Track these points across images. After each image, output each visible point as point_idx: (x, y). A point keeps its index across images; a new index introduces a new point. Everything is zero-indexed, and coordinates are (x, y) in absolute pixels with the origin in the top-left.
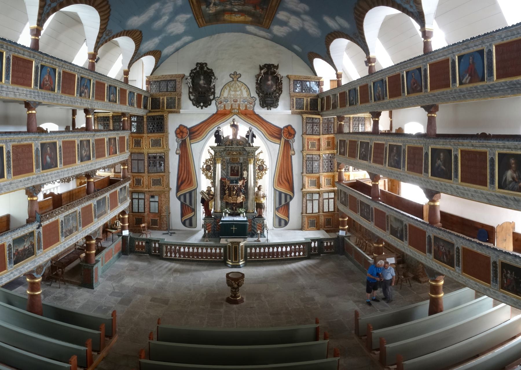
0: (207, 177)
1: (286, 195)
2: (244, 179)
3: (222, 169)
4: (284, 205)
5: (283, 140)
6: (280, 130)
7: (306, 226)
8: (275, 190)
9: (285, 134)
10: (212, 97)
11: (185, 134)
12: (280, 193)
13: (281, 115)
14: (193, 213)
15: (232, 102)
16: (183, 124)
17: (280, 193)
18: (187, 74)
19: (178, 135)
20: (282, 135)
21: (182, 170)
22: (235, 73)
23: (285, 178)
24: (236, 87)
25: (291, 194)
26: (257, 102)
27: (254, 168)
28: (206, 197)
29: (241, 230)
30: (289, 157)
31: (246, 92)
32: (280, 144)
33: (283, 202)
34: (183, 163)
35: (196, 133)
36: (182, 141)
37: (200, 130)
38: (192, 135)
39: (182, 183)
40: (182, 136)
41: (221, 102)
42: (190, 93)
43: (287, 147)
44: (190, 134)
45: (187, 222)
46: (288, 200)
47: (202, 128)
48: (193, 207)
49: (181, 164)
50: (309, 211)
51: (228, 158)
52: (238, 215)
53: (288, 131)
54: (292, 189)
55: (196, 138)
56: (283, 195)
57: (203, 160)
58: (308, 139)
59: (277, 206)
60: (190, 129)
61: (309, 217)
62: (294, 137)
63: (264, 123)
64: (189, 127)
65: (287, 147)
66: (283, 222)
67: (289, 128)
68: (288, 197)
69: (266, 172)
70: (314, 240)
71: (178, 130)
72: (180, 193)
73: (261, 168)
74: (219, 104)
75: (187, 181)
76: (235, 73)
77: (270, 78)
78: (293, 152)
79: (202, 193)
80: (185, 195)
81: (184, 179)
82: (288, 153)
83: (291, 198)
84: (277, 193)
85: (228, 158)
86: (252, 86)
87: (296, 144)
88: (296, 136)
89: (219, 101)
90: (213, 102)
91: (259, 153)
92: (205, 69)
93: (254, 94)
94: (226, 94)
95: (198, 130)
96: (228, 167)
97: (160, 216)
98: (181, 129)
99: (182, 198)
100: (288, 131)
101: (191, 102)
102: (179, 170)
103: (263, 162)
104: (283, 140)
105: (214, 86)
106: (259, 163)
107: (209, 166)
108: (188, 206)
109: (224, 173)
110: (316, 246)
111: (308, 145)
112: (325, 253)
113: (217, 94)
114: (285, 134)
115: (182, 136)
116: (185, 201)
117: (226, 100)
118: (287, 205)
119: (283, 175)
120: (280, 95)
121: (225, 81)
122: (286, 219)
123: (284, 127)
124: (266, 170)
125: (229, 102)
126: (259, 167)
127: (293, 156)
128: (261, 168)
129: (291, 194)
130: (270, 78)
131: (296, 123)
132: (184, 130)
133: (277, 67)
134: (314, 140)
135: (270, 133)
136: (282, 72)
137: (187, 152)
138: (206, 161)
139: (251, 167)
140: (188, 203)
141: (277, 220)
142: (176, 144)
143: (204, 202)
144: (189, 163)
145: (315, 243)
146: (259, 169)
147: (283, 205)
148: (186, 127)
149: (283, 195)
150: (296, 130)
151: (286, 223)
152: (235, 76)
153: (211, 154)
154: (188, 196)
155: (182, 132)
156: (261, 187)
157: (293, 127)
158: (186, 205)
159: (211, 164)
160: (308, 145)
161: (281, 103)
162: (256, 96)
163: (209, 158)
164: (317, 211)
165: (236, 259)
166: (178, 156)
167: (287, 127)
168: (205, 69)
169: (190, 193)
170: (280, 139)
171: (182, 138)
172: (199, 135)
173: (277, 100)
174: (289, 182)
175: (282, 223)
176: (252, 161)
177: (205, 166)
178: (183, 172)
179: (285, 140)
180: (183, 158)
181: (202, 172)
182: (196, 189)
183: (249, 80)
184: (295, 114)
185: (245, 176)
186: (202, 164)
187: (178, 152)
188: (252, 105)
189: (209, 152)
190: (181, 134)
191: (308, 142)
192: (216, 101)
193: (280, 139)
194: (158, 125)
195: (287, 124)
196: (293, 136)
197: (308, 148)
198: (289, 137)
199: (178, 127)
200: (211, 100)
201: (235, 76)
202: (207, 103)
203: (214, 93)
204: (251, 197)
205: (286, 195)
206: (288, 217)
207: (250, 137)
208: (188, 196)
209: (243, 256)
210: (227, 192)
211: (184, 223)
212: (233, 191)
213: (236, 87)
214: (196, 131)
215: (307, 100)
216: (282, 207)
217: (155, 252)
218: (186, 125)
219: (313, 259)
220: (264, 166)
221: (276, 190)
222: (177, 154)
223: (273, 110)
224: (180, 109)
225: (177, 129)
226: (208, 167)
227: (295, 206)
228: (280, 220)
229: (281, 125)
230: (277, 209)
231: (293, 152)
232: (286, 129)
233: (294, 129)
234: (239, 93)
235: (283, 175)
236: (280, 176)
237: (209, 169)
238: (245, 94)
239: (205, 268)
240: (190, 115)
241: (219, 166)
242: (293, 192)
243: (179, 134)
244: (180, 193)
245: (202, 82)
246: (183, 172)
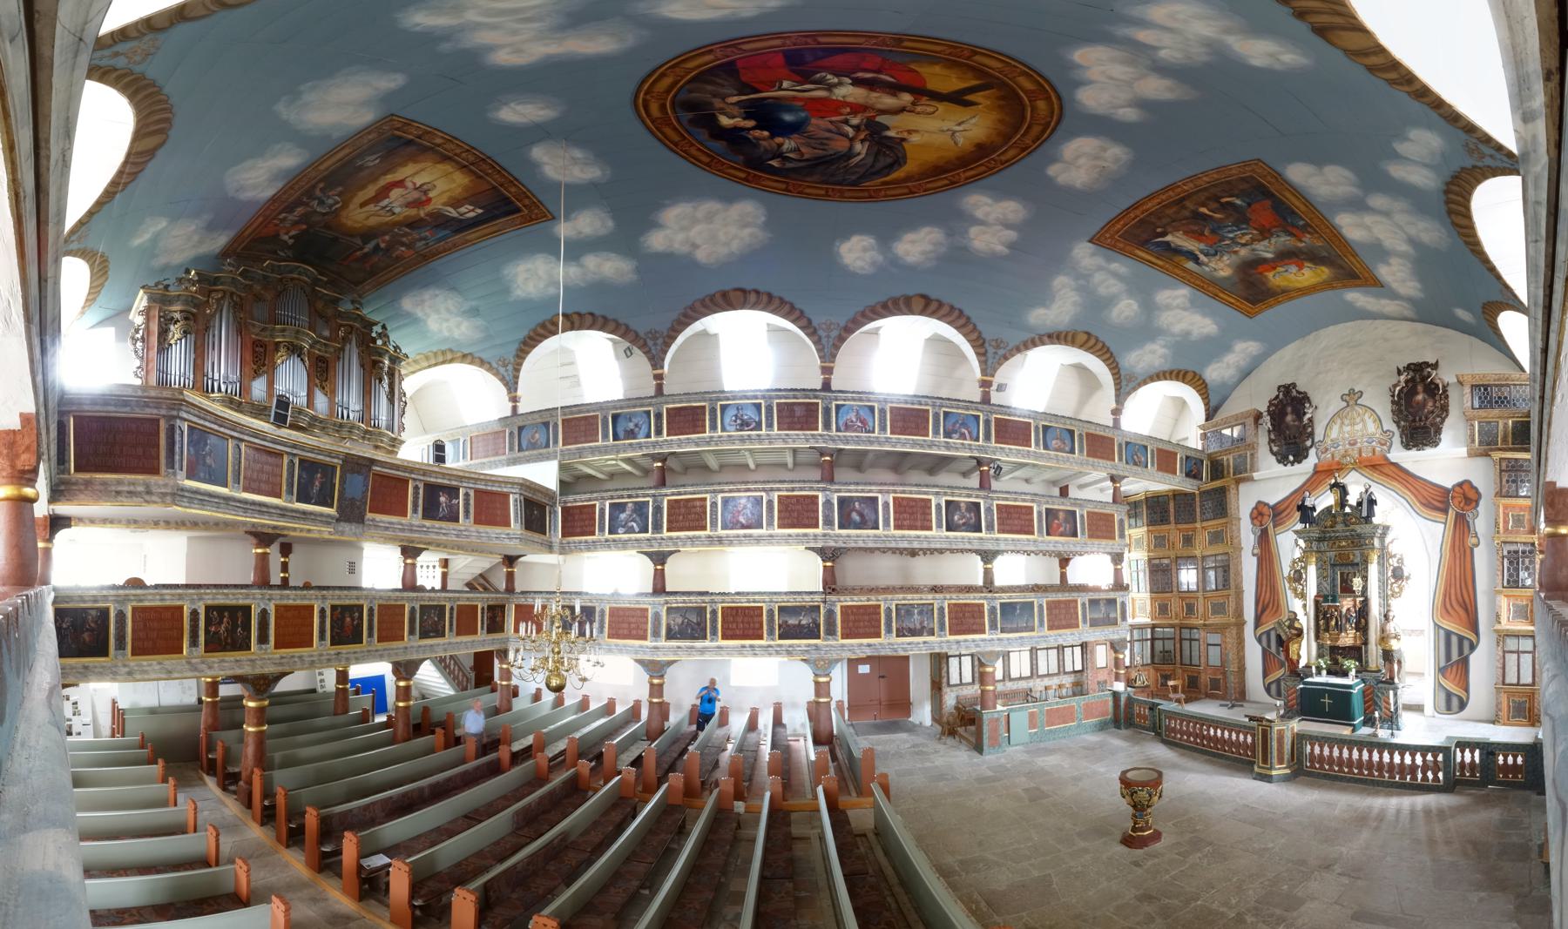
1: (1461, 639)
3: (1321, 577)
5: (1451, 514)
6: (1446, 491)
7: (1504, 714)
8: (1437, 627)
10: (1309, 443)
12: (1448, 634)
13: (1447, 459)
17: (1448, 634)
18: (1263, 408)
20: (1452, 504)
22: (1352, 392)
23: (1458, 599)
24: (1354, 420)
25: (1472, 637)
26: (1397, 439)
27: (1382, 572)
29: (1335, 706)
31: (1373, 424)
33: (1455, 656)
39: (1263, 611)
42: (1271, 441)
43: (1462, 526)
44: (1275, 516)
45: (1274, 687)
46: (1466, 651)
50: (1511, 678)
51: (1332, 554)
52: (1345, 674)
54: (1474, 627)
56: (1454, 640)
58: (1506, 507)
59: (1443, 664)
60: (1274, 508)
61: (1510, 694)
63: (1411, 480)
64: (1272, 502)
65: (1462, 526)
66: (1455, 702)
67: (1466, 487)
68: (1466, 645)
70: (1463, 745)
72: (1261, 630)
76: (1352, 392)
77: (1420, 388)
78: (1474, 540)
80: (1268, 633)
82: (1463, 541)
83: (1473, 647)
84: (1442, 632)
85: (1332, 554)
86: (1384, 409)
87: (1481, 523)
88: (1482, 503)
90: (1312, 452)
92: (1294, 393)
93: (1390, 425)
94: (1334, 433)
96: (1334, 573)
97: (1224, 673)
101: (1273, 458)
104: (1451, 514)
105: (1310, 420)
106: (1394, 562)
110: (1477, 759)
111: (1506, 522)
112: (1500, 783)
113: (1318, 436)
117: (1335, 444)
118: (1464, 663)
120: (1443, 421)
121: (1333, 409)
122: (1463, 695)
129: (1472, 637)
130: (1420, 388)
131: (1481, 474)
132: (1265, 510)
133: (1435, 366)
134: (1521, 508)
136: (1446, 376)
137: (1269, 551)
138: (1294, 562)
139: (1373, 569)
141: (1443, 696)
145: (1472, 753)
146: (1394, 576)
147: (1455, 664)
149: (1454, 640)
151: (1463, 705)
152: (1352, 398)
155: (1261, 514)
160: (1506, 522)
161: (1447, 435)
162: (1394, 428)
164: (1530, 680)
165: (1265, 761)
167: (1460, 485)
168: (1294, 393)
170: (1445, 511)
173: (1438, 431)
174: (1466, 610)
175: (1454, 703)
183: (1378, 402)
191: (1506, 515)
193: (1445, 511)
194: (1219, 503)
197: (1506, 530)
200: (1307, 449)
201: (1352, 398)
202: (1300, 456)
203: (1312, 435)
204: (1373, 635)
205: (1461, 639)
206: (1467, 690)
209: (1286, 757)
211: (1268, 690)
213: (1354, 420)
215: (1506, 425)
217: (1381, 775)
219: (1459, 793)
223: (1429, 452)
227: (1481, 664)
228: (1449, 695)
230: (1442, 671)
231: (1474, 540)
234: (1359, 427)
236: (1446, 594)
238: (1372, 427)
240: (1274, 480)
241: (1312, 571)
242: (1477, 633)
244: (1261, 630)
245: (1289, 418)
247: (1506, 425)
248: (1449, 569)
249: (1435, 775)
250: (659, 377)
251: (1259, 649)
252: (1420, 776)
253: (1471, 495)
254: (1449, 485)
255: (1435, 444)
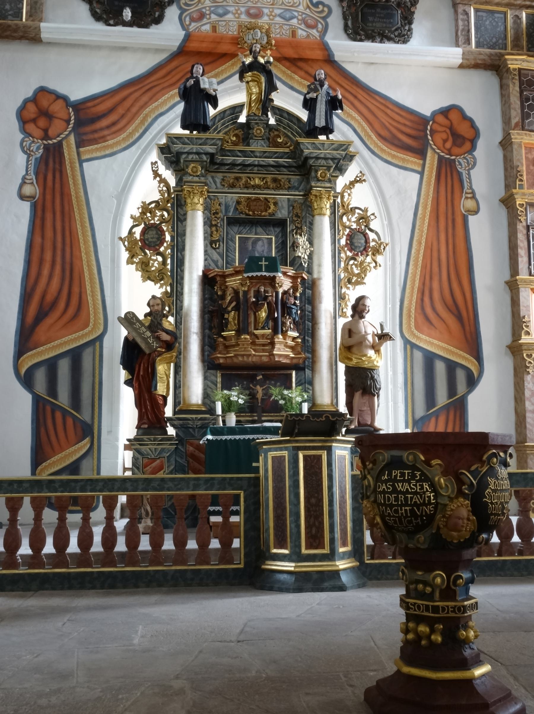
0: (148, 275)
1: (452, 367)
2: (295, 262)
4: (447, 407)
5: (431, 159)
6: (420, 121)
9: (439, 138)
11: (57, 126)
12: (430, 359)
14: (85, 444)
15: (244, 17)
16: (52, 85)
17: (430, 359)
19: (31, 127)
21: (41, 261)
26: (336, 21)
28: (145, 339)
30: (459, 221)
32: (422, 173)
33: (442, 398)
34: (49, 233)
35: (104, 123)
36: (47, 148)
37: (121, 110)
38: (88, 129)
39: (42, 314)
40: (46, 131)
41: (202, 16)
43: (449, 181)
44: (80, 123)
46: (461, 388)
47: (127, 104)
48: (86, 416)
49: (38, 240)
53: (451, 128)
55: (104, 139)
56: (440, 368)
57: (133, 208)
60: (79, 107)
62: (473, 147)
63: (361, 95)
64: (76, 94)
65: (449, 181)
67: (453, 116)
68: (461, 376)
69: (379, 259)
71: (32, 108)
72: (29, 360)
73: (359, 244)
74: (192, 20)
75: (62, 305)
78: (470, 204)
79: (129, 320)
80: (51, 365)
81: (49, 298)
82: (452, 204)
83: (472, 382)
84: (418, 356)
85: (231, 198)
87: (483, 175)
88: (481, 144)
89: (193, 9)
91: (352, 184)
95: (111, 110)
98: (44, 103)
99: (40, 377)
100: (451, 128)
102: (28, 262)
103: (364, 219)
106: (351, 222)
107: (157, 228)
108: (65, 412)
109: (216, 256)
114: (439, 138)
115: (46, 131)
116: (52, 390)
119: (436, 285)
123: (435, 114)
124: (377, 251)
125: (230, 17)
126: (350, 237)
127: (471, 219)
128: (360, 241)
131: (478, 100)
132: (57, 107)
135: (383, 133)
137: (64, 194)
139: (324, 224)
140: (64, 398)
142: (21, 159)
143: (138, 362)
144: (73, 235)
148: (65, 99)
149: (440, 368)
150: (479, 123)
153: (163, 181)
154: (64, 368)
155: (46, 114)
156: (368, 302)
157: (469, 113)
158: (55, 408)
159: (163, 220)
161: (420, 28)
163: (157, 197)
166: (26, 207)
167: (445, 112)
169: (75, 356)
170: (421, 153)
171: (46, 137)
172: (116, 128)
173: (408, 19)
174: (459, 317)
176: (327, 205)
177: (138, 231)
178: (46, 272)
179: (441, 159)
180: (49, 216)
181: (125, 255)
182: (100, 338)
184: (476, 66)
185: (302, 253)
186: (127, 224)
187: (28, 190)
188: (314, 32)
189: (156, 174)
190: (42, 122)
192: (183, 11)
193: (421, 153)
195: (445, 103)
196: (468, 145)
198: (456, 150)
199: (30, 94)
205: (452, 367)
207: (321, 108)
208: (64, 368)
210: (232, 316)
212: (257, 306)
214: (104, 115)
216: (437, 415)
218: (61, 89)
220: (372, 236)
221: (414, 346)
222: (22, 197)
224: (41, 20)
225: (26, 102)
226: (152, 234)
229: (426, 106)
231: (470, 204)
232: (441, 119)
233: (471, 122)
235: (436, 285)
236: (424, 291)
237: (157, 241)
239: (200, 337)
242: (478, 356)
243: (34, 121)
244: (29, 360)
246: (46, 272)
247: (517, 18)
248: (429, 248)
249: (226, 544)
250: (489, 632)
251: (25, 400)
252: (192, 545)
253: (463, 129)
254: (427, 112)
255: (403, 37)
